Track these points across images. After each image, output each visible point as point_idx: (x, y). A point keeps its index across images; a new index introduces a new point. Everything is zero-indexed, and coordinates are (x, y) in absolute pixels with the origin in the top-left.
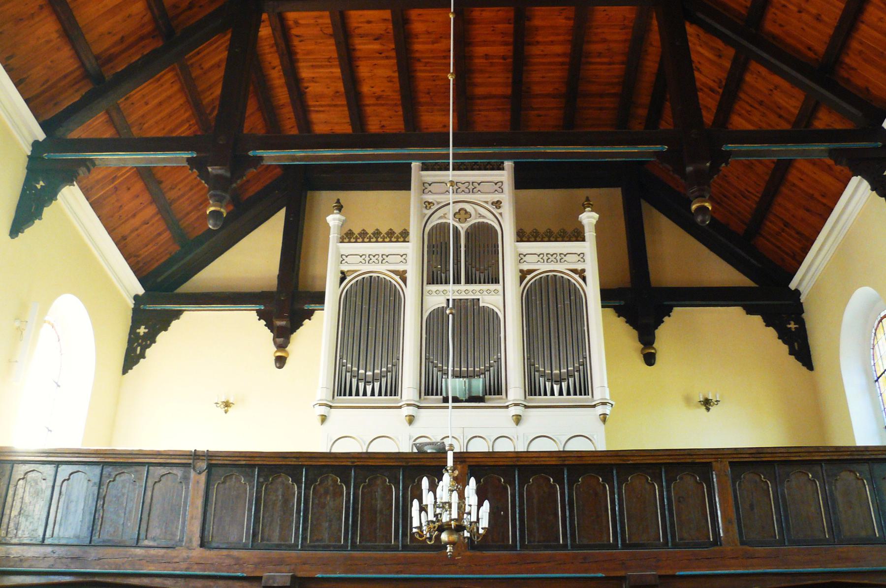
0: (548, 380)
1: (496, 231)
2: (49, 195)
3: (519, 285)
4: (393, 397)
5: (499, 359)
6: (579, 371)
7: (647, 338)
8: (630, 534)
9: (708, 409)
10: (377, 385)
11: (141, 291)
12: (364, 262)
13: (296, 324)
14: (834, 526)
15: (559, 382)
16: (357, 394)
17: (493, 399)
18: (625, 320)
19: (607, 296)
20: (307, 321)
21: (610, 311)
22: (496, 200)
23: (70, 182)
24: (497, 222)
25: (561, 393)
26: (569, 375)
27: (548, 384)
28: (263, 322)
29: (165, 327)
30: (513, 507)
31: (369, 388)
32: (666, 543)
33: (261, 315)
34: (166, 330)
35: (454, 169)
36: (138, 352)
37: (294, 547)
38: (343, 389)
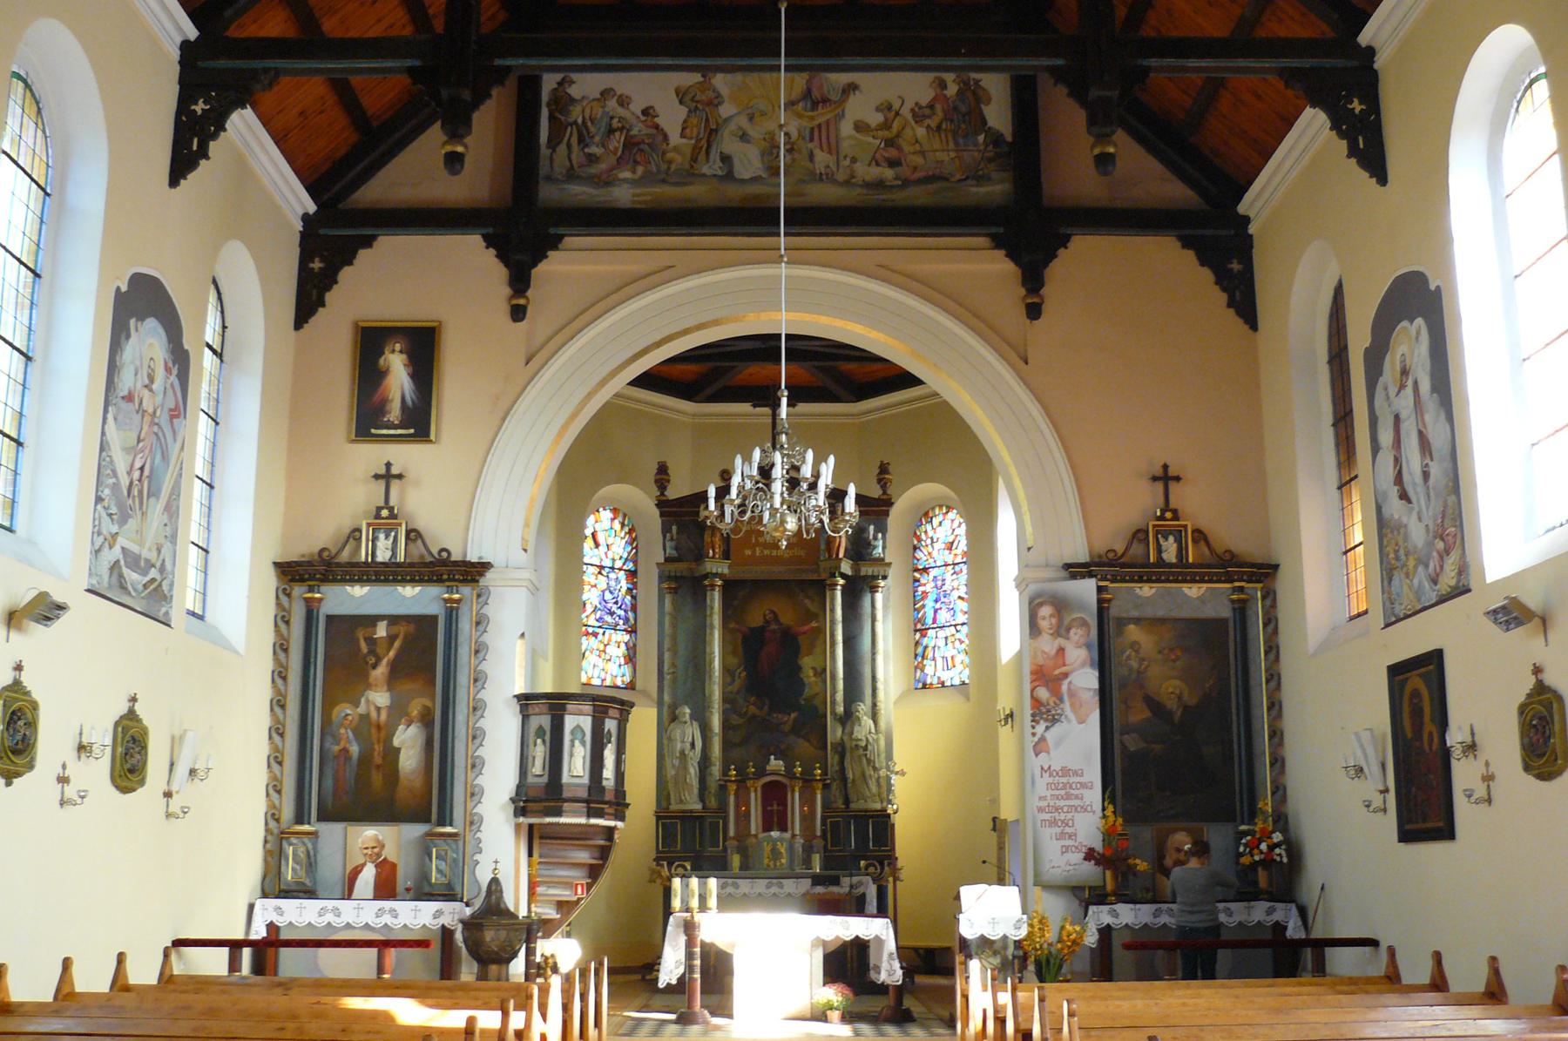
2: (215, 123)
3: (789, 1016)
28: (492, 251)
33: (490, 241)
35: (780, 335)
36: (314, 298)
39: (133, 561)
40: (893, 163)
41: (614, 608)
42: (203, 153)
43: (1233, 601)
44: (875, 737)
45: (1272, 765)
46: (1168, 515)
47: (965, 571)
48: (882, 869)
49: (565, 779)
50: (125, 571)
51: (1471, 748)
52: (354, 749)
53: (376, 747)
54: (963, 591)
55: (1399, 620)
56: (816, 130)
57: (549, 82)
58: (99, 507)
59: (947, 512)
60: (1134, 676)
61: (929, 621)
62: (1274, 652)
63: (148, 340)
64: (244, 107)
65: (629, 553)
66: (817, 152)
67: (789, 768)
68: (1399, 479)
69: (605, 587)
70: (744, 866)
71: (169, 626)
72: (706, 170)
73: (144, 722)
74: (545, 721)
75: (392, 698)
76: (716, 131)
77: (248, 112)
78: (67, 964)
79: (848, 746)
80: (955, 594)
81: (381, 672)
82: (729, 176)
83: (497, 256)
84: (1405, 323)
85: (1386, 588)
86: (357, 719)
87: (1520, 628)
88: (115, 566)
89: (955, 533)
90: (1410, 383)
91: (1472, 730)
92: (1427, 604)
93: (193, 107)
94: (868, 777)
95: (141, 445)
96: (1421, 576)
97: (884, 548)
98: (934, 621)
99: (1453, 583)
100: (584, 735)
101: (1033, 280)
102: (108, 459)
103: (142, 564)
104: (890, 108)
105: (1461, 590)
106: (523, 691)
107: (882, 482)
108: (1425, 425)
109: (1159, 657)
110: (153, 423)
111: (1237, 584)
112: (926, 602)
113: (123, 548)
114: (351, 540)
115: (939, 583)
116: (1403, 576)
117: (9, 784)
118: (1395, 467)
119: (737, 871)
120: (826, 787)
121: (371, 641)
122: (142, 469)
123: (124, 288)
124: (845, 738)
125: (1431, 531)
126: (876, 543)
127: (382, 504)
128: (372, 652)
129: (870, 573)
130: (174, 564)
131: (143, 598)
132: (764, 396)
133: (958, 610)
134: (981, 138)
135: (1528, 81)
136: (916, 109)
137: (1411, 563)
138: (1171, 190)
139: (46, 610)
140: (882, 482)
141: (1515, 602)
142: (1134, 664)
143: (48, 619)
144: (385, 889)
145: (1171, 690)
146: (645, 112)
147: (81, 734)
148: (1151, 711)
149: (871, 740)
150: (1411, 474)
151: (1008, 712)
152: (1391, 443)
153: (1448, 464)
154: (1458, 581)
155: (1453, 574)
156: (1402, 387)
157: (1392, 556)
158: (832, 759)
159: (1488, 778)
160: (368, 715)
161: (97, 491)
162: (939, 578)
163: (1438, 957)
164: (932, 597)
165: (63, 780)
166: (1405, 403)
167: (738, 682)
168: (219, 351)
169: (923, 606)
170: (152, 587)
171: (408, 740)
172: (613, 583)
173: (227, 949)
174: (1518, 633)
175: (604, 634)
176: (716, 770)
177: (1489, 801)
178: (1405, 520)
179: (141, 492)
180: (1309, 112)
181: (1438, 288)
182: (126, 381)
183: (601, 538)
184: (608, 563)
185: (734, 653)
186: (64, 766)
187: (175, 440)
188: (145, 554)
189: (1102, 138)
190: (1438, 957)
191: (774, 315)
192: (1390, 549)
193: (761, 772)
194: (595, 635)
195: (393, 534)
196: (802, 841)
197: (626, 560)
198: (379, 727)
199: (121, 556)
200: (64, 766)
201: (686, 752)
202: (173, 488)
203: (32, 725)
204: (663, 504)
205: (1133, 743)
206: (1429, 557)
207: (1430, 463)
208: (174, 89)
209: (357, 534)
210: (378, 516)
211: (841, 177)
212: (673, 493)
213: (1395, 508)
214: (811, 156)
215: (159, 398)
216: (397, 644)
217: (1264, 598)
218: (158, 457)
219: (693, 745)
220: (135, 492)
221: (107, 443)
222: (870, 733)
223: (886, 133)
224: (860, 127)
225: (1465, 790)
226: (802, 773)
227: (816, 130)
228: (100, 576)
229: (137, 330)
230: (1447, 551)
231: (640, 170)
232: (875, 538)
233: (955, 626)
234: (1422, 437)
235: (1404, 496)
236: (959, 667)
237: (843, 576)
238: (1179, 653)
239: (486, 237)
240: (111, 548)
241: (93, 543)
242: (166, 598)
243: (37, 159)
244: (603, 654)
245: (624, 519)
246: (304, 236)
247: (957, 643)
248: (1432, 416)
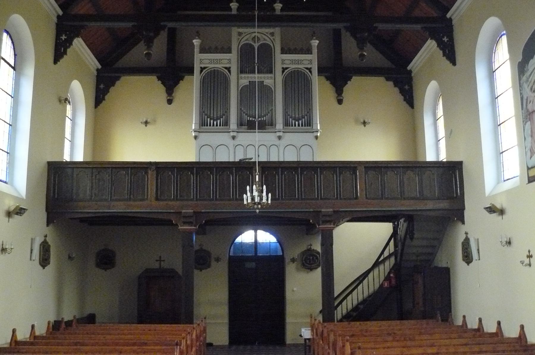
0: (294, 119)
1: (270, 46)
2: (69, 42)
4: (226, 127)
5: (272, 110)
6: (307, 116)
7: (339, 91)
8: (324, 194)
9: (365, 126)
10: (219, 121)
11: (100, 67)
12: (211, 62)
13: (176, 83)
14: (402, 193)
15: (298, 121)
16: (210, 125)
17: (269, 128)
18: (330, 82)
19: (321, 71)
20: (181, 81)
21: (323, 78)
22: (271, 32)
23: (78, 36)
24: (271, 42)
25: (299, 125)
26: (303, 117)
27: (293, 122)
28: (160, 82)
29: (113, 84)
30: (279, 183)
31: (215, 123)
32: (337, 198)
33: (159, 78)
34: (114, 86)
36: (101, 97)
37: (192, 200)
38: (203, 123)
42: (65, 53)
78: (14, 331)
83: (162, 83)
87: (494, 214)
93: (61, 38)
138: (385, 63)
143: (20, 213)
147: (3, 245)
180: (429, 41)
189: (361, 49)
191: (255, 30)
208: (54, 32)
225: (521, 262)
243: (11, 58)
246: (98, 76)
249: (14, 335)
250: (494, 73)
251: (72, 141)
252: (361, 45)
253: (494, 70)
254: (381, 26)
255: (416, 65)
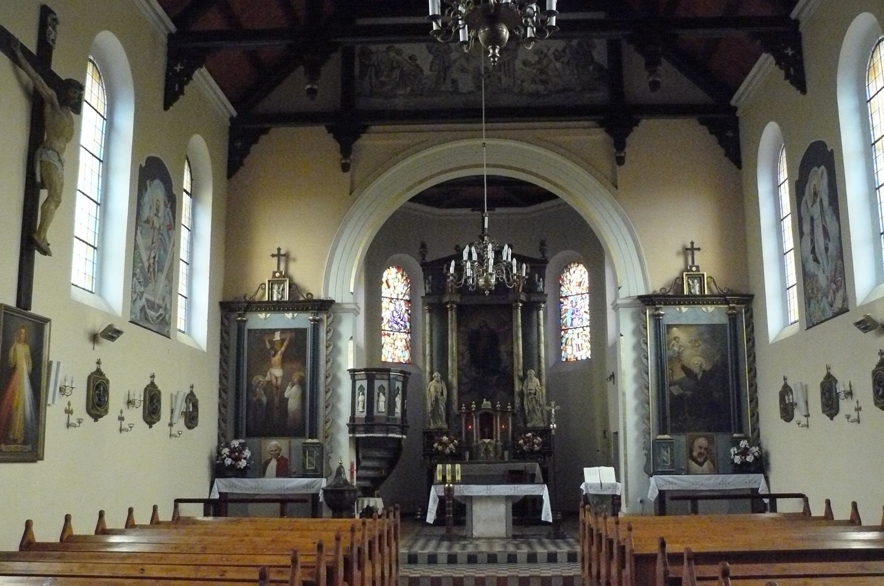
28: (331, 135)
29: (255, 141)
33: (330, 130)
39: (152, 305)
40: (544, 82)
41: (399, 320)
42: (181, 92)
43: (729, 315)
44: (540, 388)
45: (751, 402)
46: (694, 269)
47: (588, 298)
48: (545, 458)
49: (375, 413)
50: (148, 311)
51: (850, 394)
52: (264, 399)
53: (276, 398)
54: (587, 308)
55: (814, 325)
56: (502, 66)
57: (358, 49)
58: (135, 279)
59: (578, 266)
60: (676, 355)
61: (569, 325)
62: (752, 341)
63: (156, 192)
64: (202, 67)
65: (406, 291)
66: (503, 77)
67: (494, 405)
68: (813, 251)
69: (393, 309)
70: (471, 458)
71: (169, 338)
72: (443, 88)
73: (159, 388)
74: (364, 383)
75: (283, 371)
76: (449, 67)
77: (204, 70)
78: (101, 514)
79: (525, 392)
80: (583, 310)
81: (277, 358)
82: (456, 91)
83: (334, 137)
84: (816, 168)
85: (808, 309)
86: (265, 383)
88: (143, 309)
89: (582, 277)
90: (818, 200)
91: (850, 384)
92: (828, 317)
94: (536, 410)
95: (154, 245)
96: (824, 303)
97: (544, 286)
98: (572, 325)
99: (840, 306)
100: (384, 389)
101: (620, 144)
102: (138, 254)
103: (156, 307)
104: (542, 52)
105: (844, 310)
106: (352, 368)
107: (543, 251)
108: (826, 224)
109: (690, 344)
110: (159, 233)
111: (731, 305)
112: (567, 314)
113: (146, 299)
114: (260, 289)
115: (574, 304)
116: (815, 301)
117: (150, 427)
118: (811, 244)
119: (468, 460)
120: (514, 415)
121: (272, 343)
122: (154, 258)
123: (144, 165)
124: (524, 389)
125: (829, 279)
126: (539, 284)
127: (276, 270)
128: (272, 348)
129: (536, 300)
130: (171, 306)
131: (156, 324)
132: (475, 204)
133: (584, 318)
134: (591, 68)
135: (877, 41)
136: (556, 53)
137: (820, 296)
138: (695, 94)
139: (112, 334)
140: (543, 251)
141: (868, 318)
142: (676, 349)
144: (283, 471)
145: (696, 362)
146: (410, 58)
148: (686, 373)
149: (537, 389)
150: (819, 249)
151: (611, 374)
152: (809, 231)
153: (837, 244)
154: (843, 305)
155: (841, 301)
156: (814, 202)
157: (810, 291)
158: (517, 400)
159: (858, 409)
160: (271, 381)
161: (133, 271)
162: (574, 301)
163: (828, 502)
164: (570, 312)
165: (121, 419)
166: (816, 211)
167: (465, 362)
168: (190, 192)
169: (566, 317)
170: (161, 318)
171: (292, 393)
172: (398, 307)
173: (203, 504)
174: (871, 334)
175: (393, 334)
176: (455, 406)
177: (808, 426)
178: (816, 273)
179: (154, 269)
180: (764, 56)
181: (832, 150)
182: (146, 213)
183: (390, 283)
184: (395, 296)
185: (464, 345)
186: (121, 412)
187: (170, 242)
188: (157, 301)
189: (653, 72)
190: (828, 502)
192: (809, 288)
193: (478, 408)
194: (389, 335)
195: (282, 286)
196: (501, 444)
197: (405, 294)
198: (277, 388)
199: (146, 303)
200: (121, 412)
201: (439, 397)
202: (170, 267)
203: (106, 391)
204: (424, 265)
205: (676, 390)
206: (828, 292)
207: (829, 243)
209: (263, 286)
210: (274, 276)
211: (516, 91)
212: (428, 259)
213: (811, 266)
214: (500, 79)
215: (162, 220)
216: (285, 343)
217: (746, 313)
218: (162, 252)
219: (442, 394)
220: (152, 270)
221: (138, 245)
222: (537, 386)
223: (539, 66)
224: (525, 63)
226: (500, 408)
227: (502, 66)
228: (136, 314)
229: (150, 186)
230: (837, 290)
231: (409, 89)
232: (539, 281)
233: (583, 327)
234: (824, 228)
235: (816, 260)
236: (585, 350)
237: (522, 302)
238: (700, 342)
239: (327, 127)
240: (140, 299)
241: (132, 297)
242: (168, 324)
243: (99, 101)
244: (393, 345)
245: (403, 273)
247: (584, 336)
248: (829, 219)
249: (68, 525)
250: (869, 104)
251: (192, 230)
252: (652, 64)
253: (868, 99)
254: (685, 34)
255: (742, 98)
